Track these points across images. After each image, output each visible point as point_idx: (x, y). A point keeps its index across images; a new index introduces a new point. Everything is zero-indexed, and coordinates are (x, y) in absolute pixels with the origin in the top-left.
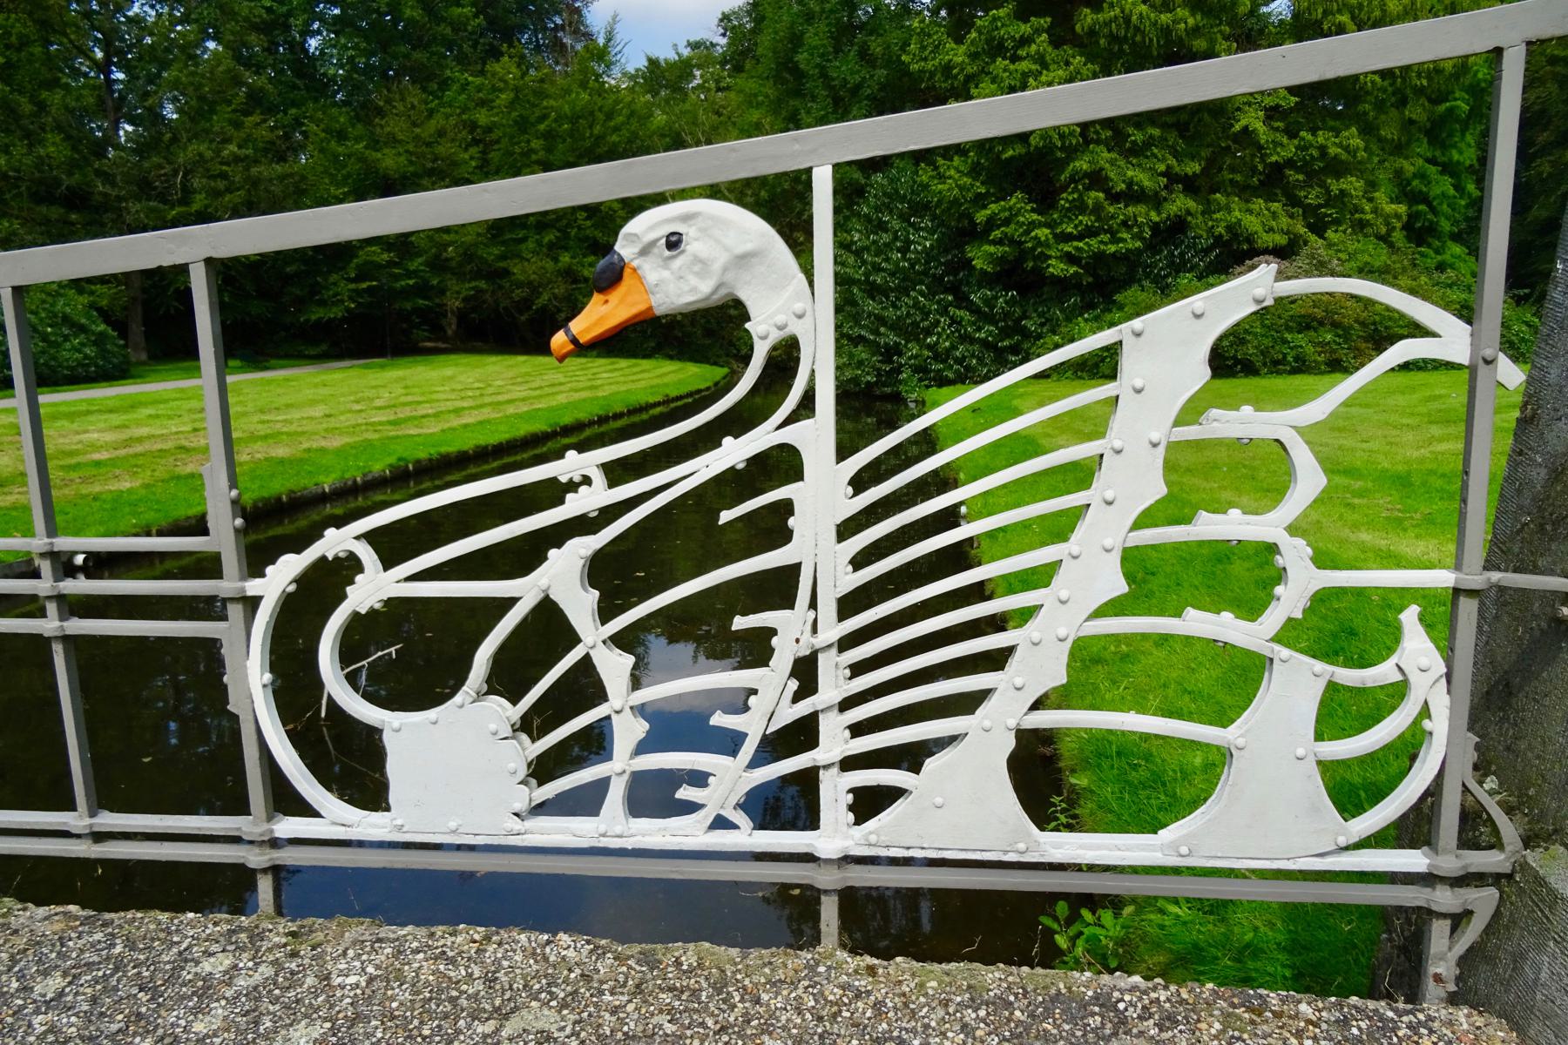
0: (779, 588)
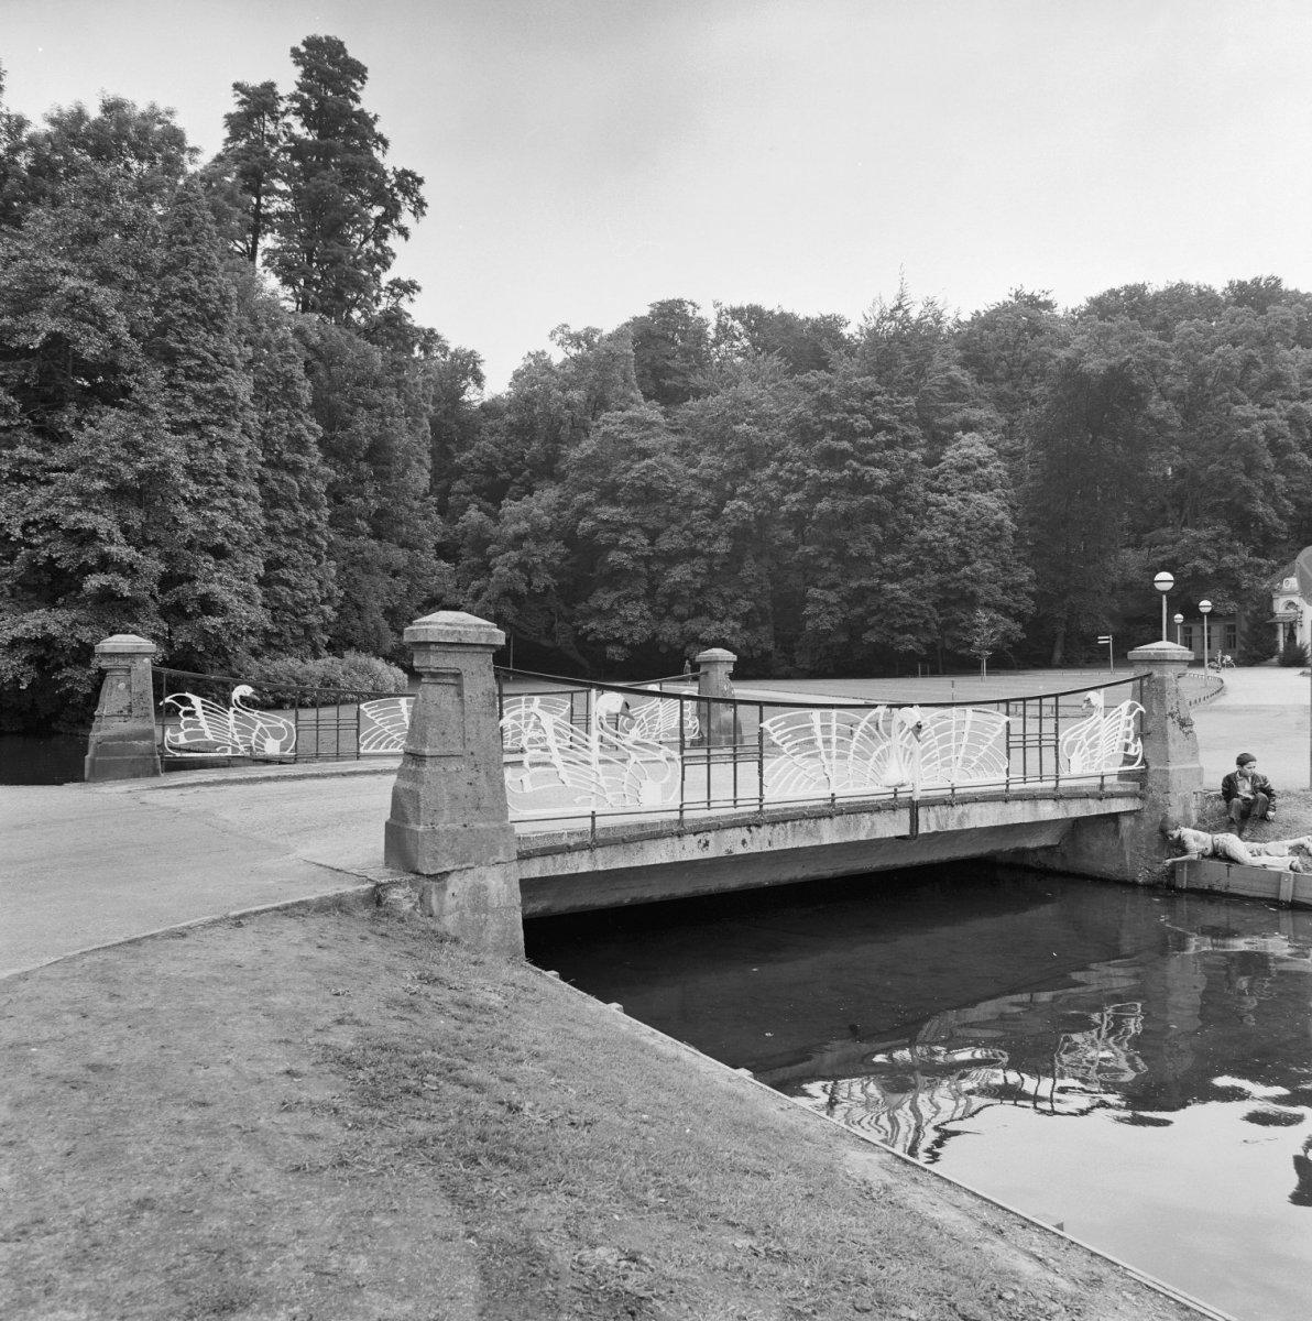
0: (1098, 739)
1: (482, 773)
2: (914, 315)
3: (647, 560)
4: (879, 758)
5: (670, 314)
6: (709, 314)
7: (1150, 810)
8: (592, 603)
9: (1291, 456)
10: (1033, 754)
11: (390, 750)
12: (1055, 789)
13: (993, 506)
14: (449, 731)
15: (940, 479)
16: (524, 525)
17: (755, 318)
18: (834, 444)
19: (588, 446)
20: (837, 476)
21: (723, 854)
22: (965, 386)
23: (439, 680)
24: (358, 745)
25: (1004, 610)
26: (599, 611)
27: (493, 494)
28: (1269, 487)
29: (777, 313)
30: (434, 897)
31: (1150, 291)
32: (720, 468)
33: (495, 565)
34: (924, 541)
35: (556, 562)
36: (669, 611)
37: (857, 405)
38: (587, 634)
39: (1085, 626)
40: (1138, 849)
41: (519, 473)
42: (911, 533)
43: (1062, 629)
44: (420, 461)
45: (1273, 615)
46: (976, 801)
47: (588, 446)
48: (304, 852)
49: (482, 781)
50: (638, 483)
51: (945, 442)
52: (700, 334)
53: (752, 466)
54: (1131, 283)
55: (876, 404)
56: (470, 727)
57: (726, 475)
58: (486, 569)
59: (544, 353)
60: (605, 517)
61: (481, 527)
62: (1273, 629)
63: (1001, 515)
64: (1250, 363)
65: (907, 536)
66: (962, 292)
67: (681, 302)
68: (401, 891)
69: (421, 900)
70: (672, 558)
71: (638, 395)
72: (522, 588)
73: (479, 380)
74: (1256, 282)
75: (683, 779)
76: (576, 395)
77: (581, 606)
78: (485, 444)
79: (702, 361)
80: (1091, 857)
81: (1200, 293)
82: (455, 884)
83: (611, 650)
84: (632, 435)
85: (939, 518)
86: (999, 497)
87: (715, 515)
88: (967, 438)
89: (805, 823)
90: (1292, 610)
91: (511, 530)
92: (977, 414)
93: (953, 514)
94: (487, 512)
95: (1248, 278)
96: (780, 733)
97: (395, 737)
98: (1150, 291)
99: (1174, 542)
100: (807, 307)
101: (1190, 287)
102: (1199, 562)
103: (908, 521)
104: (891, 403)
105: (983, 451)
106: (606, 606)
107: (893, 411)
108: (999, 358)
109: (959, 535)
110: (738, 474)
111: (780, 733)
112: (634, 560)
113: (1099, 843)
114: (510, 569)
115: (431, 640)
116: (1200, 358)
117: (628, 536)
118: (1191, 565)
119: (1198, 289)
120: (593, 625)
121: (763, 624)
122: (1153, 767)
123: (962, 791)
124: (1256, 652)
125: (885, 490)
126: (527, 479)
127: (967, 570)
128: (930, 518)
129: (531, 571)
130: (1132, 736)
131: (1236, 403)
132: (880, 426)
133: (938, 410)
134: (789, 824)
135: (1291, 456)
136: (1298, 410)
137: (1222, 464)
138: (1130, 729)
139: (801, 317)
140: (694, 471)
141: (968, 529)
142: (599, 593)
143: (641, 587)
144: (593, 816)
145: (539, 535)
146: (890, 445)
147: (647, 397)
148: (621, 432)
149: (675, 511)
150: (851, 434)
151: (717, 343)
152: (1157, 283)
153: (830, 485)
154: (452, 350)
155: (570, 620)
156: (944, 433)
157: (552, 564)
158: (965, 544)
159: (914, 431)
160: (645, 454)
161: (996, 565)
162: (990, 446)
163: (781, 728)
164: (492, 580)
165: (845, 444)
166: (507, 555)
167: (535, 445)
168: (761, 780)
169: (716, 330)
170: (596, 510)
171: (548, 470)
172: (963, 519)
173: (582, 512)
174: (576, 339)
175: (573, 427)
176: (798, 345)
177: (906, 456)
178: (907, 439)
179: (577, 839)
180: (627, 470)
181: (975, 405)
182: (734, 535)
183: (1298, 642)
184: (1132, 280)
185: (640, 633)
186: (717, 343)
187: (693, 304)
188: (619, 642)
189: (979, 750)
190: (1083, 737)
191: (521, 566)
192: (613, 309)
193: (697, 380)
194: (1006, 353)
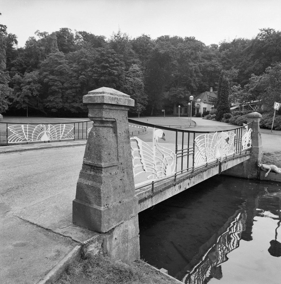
1: (126, 174)
2: (122, 37)
3: (61, 89)
5: (64, 31)
6: (74, 32)
8: (48, 99)
9: (199, 74)
11: (18, 142)
12: (240, 155)
13: (140, 81)
14: (112, 153)
15: (129, 74)
16: (31, 79)
17: (85, 35)
18: (105, 64)
19: (45, 61)
20: (105, 71)
21: (184, 190)
22: (133, 54)
23: (105, 125)
24: (7, 141)
25: (142, 104)
26: (50, 101)
27: (22, 72)
28: (194, 80)
29: (90, 34)
30: (108, 243)
31: (170, 37)
32: (78, 68)
33: (23, 89)
34: (125, 88)
35: (39, 88)
36: (67, 101)
37: (110, 56)
38: (47, 106)
41: (28, 66)
42: (122, 86)
44: (4, 61)
45: (195, 106)
47: (45, 61)
48: (17, 209)
49: (125, 178)
50: (59, 70)
51: (129, 66)
52: (72, 36)
53: (86, 68)
54: (166, 35)
55: (114, 56)
56: (120, 150)
57: (79, 70)
58: (20, 89)
59: (34, 37)
60: (51, 78)
61: (19, 79)
63: (142, 83)
64: (192, 53)
65: (121, 86)
66: (133, 34)
67: (67, 29)
68: (93, 245)
69: (102, 246)
70: (67, 89)
71: (58, 50)
72: (30, 95)
73: (16, 42)
74: (190, 37)
75: (177, 163)
76: (42, 48)
77: (45, 100)
78: (19, 58)
79: (72, 43)
81: (180, 39)
82: (116, 234)
83: (52, 110)
84: (57, 59)
85: (128, 83)
86: (141, 79)
87: (78, 79)
88: (134, 65)
90: (198, 106)
91: (28, 80)
92: (136, 60)
93: (131, 82)
94: (21, 76)
95: (189, 37)
97: (20, 138)
98: (170, 37)
99: (176, 90)
100: (97, 33)
101: (178, 37)
102: (181, 95)
103: (121, 83)
104: (118, 56)
105: (138, 69)
106: (52, 100)
107: (118, 58)
108: (140, 48)
109: (132, 87)
110: (82, 70)
112: (58, 89)
114: (27, 90)
115: (105, 102)
116: (183, 52)
117: (56, 83)
118: (179, 95)
119: (179, 37)
120: (48, 104)
123: (228, 157)
125: (116, 76)
126: (31, 68)
127: (135, 94)
128: (126, 83)
129: (32, 91)
130: (250, 138)
131: (189, 62)
132: (115, 61)
133: (128, 58)
135: (199, 74)
136: (200, 64)
137: (186, 75)
139: (96, 36)
140: (72, 68)
141: (135, 85)
142: (50, 96)
143: (60, 95)
144: (153, 183)
145: (35, 82)
146: (117, 65)
147: (60, 51)
148: (55, 58)
149: (68, 78)
150: (109, 63)
151: (76, 40)
152: (171, 36)
153: (104, 74)
154: (8, 34)
155: (42, 103)
156: (129, 64)
157: (38, 89)
158: (134, 89)
159: (123, 63)
160: (60, 64)
161: (140, 94)
162: (139, 67)
164: (22, 92)
165: (107, 65)
166: (26, 86)
167: (32, 60)
168: (193, 161)
169: (76, 37)
170: (49, 76)
171: (35, 66)
172: (134, 83)
173: (45, 77)
174: (41, 34)
175: (42, 56)
176: (96, 42)
177: (121, 68)
178: (121, 64)
179: (148, 194)
180: (56, 67)
181: (135, 58)
182: (81, 83)
183: (199, 112)
184: (167, 34)
185: (61, 105)
186: (76, 40)
187: (70, 29)
188: (55, 108)
191: (30, 89)
192: (52, 28)
193: (72, 47)
194: (142, 47)
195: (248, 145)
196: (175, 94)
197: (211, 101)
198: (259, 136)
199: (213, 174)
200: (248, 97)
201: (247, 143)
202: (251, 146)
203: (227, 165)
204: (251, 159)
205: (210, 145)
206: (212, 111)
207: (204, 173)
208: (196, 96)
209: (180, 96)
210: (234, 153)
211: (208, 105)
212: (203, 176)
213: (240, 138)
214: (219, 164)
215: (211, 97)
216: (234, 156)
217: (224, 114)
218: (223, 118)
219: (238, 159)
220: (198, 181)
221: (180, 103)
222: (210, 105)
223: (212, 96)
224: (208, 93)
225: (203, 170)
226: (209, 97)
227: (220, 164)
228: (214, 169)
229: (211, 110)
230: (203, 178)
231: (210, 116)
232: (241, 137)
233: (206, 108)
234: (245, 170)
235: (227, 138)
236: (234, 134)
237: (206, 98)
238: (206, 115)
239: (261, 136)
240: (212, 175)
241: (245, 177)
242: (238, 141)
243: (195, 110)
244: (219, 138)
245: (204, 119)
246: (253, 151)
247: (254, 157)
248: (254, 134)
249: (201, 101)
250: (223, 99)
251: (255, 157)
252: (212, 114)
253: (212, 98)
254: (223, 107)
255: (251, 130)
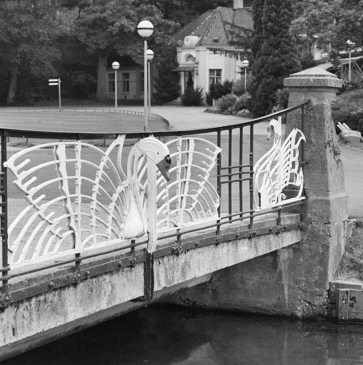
4: (117, 202)
7: (309, 242)
10: (235, 186)
12: (250, 226)
39: (35, 71)
40: (297, 282)
43: (15, 72)
45: (177, 64)
46: (197, 246)
62: (177, 76)
80: (246, 292)
89: (50, 296)
90: (190, 62)
96: (25, 174)
111: (25, 174)
113: (255, 278)
121: (147, 7)
122: (312, 197)
124: (165, 94)
130: (297, 166)
134: (34, 300)
138: (296, 159)
163: (26, 168)
168: (5, 245)
189: (198, 187)
190: (268, 168)
195: (290, 191)
196: (98, 15)
197: (238, 44)
198: (329, 156)
199: (112, 296)
200: (358, 24)
201: (282, 182)
202: (304, 194)
203: (187, 264)
204: (306, 246)
205: (87, 188)
206: (243, 79)
207: (69, 294)
208: (183, 25)
209: (122, 27)
210: (215, 218)
211: (228, 58)
212: (63, 306)
213: (246, 161)
214: (141, 258)
215: (236, 27)
216: (217, 232)
217: (279, 91)
218: (276, 105)
219: (240, 242)
220: (34, 324)
221: (121, 53)
222: (233, 59)
223: (240, 25)
224: (226, 12)
225: (58, 281)
226: (228, 27)
227: (148, 261)
228: (118, 279)
229: (239, 77)
230: (65, 314)
231: (234, 100)
232: (251, 159)
233: (219, 72)
234: (286, 288)
235: (161, 158)
236: (214, 150)
237: (218, 32)
238: (217, 98)
239: (341, 157)
240: (109, 303)
241: (287, 310)
242: (234, 175)
243: (179, 78)
244: (136, 158)
245: (211, 112)
246: (303, 211)
247: (315, 236)
248: (314, 148)
249: (200, 44)
250: (274, 35)
251: (317, 237)
252: (239, 93)
253: (242, 34)
254: (273, 63)
255: (298, 135)
